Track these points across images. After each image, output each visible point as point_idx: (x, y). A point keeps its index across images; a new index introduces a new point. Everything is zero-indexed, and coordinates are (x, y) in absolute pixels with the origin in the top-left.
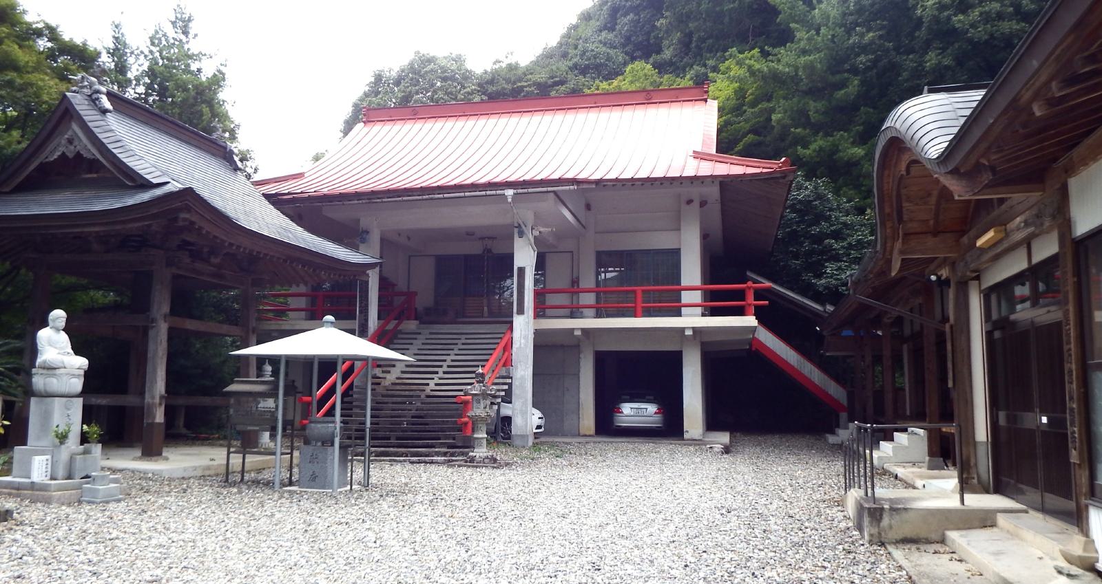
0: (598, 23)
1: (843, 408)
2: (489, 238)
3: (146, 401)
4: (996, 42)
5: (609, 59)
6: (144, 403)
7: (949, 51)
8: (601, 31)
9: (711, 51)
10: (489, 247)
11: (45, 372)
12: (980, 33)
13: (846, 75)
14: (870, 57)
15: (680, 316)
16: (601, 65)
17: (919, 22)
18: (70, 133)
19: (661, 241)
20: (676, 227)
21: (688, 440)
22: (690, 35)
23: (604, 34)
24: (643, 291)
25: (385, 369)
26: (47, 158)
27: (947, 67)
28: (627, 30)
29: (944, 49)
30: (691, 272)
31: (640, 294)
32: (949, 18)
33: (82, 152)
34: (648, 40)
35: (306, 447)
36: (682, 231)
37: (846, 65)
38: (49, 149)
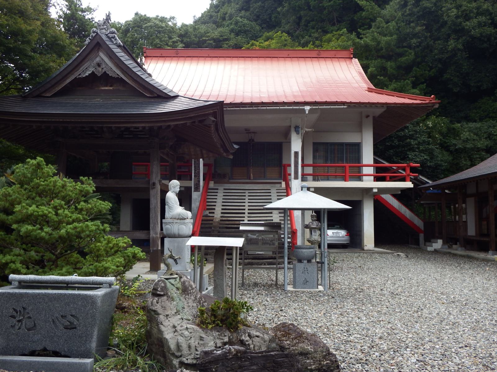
0: (238, 6)
1: (421, 231)
2: (253, 133)
3: (151, 236)
4: (483, 38)
5: (252, 28)
6: (149, 237)
7: (460, 41)
8: (240, 11)
9: (313, 28)
10: (253, 138)
11: (179, 221)
12: (476, 33)
13: (406, 49)
14: (419, 40)
15: (362, 181)
16: (248, 31)
17: (445, 23)
18: (98, 59)
19: (351, 138)
20: (359, 129)
21: (367, 250)
22: (300, 18)
23: (243, 12)
24: (350, 166)
25: (211, 211)
26: (80, 75)
27: (459, 49)
28: (258, 12)
29: (458, 39)
30: (368, 156)
31: (348, 168)
32: (461, 23)
33: (107, 72)
34: (270, 18)
35: (299, 264)
36: (363, 133)
37: (404, 44)
38: (81, 69)
